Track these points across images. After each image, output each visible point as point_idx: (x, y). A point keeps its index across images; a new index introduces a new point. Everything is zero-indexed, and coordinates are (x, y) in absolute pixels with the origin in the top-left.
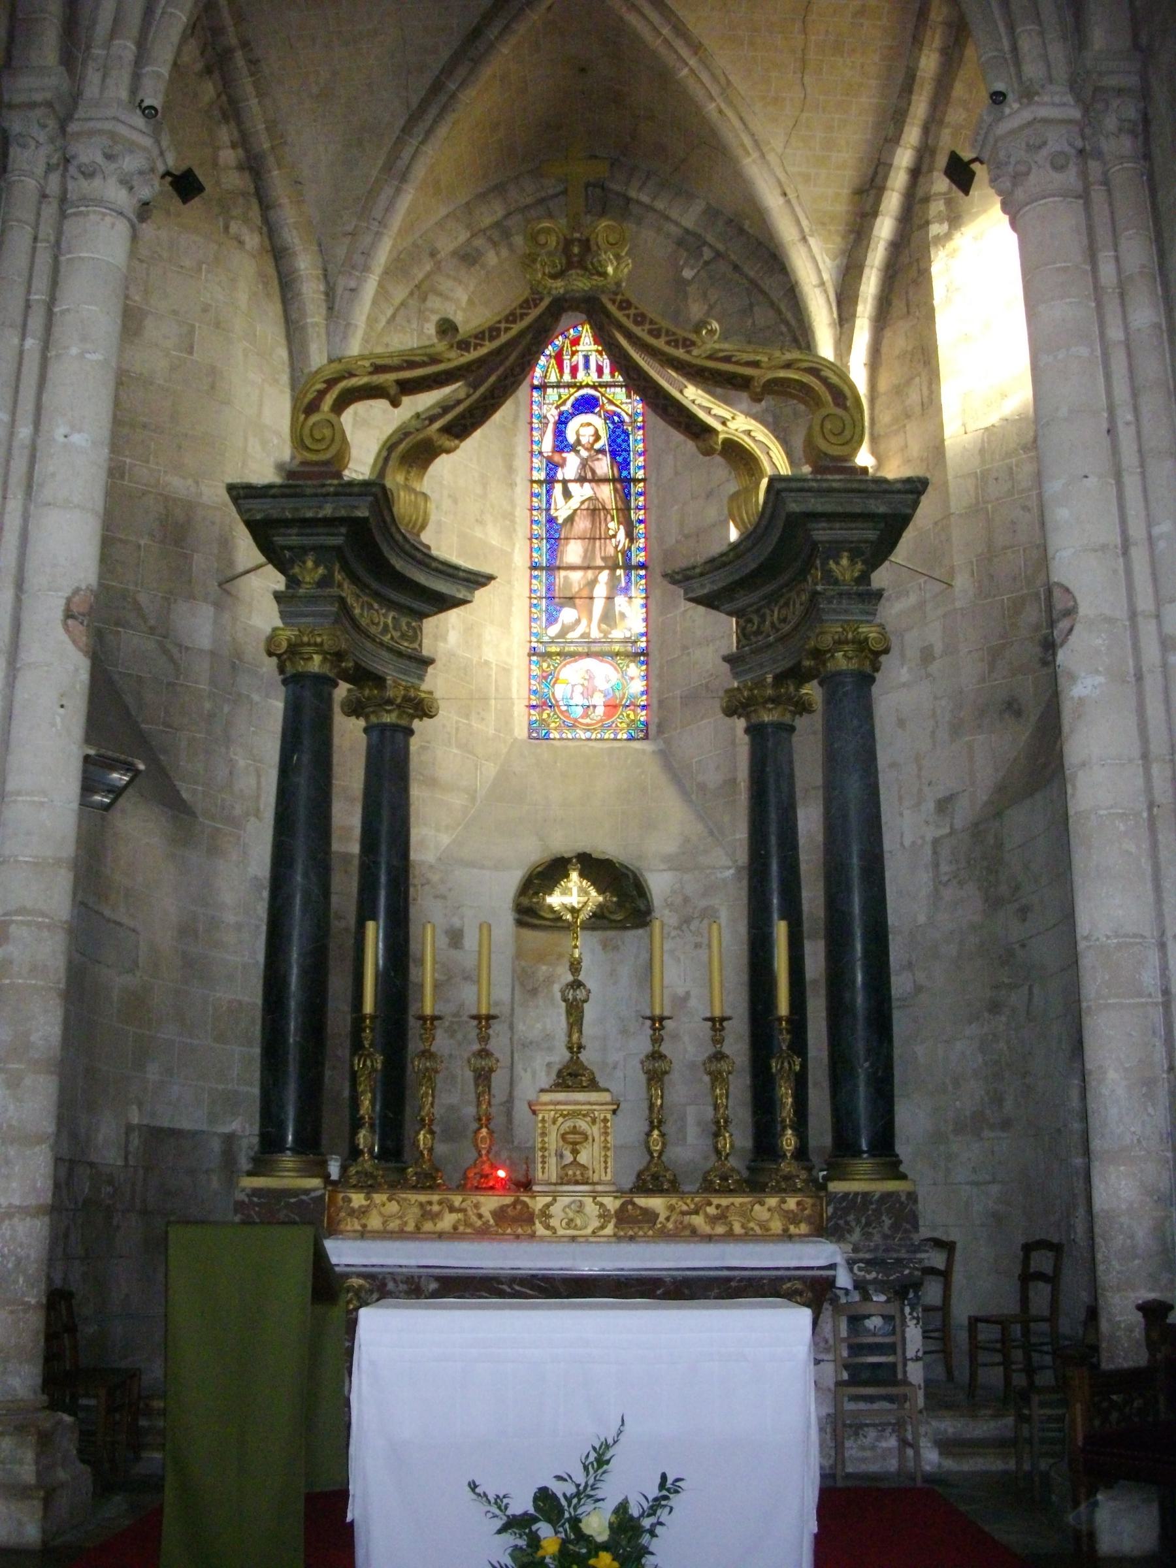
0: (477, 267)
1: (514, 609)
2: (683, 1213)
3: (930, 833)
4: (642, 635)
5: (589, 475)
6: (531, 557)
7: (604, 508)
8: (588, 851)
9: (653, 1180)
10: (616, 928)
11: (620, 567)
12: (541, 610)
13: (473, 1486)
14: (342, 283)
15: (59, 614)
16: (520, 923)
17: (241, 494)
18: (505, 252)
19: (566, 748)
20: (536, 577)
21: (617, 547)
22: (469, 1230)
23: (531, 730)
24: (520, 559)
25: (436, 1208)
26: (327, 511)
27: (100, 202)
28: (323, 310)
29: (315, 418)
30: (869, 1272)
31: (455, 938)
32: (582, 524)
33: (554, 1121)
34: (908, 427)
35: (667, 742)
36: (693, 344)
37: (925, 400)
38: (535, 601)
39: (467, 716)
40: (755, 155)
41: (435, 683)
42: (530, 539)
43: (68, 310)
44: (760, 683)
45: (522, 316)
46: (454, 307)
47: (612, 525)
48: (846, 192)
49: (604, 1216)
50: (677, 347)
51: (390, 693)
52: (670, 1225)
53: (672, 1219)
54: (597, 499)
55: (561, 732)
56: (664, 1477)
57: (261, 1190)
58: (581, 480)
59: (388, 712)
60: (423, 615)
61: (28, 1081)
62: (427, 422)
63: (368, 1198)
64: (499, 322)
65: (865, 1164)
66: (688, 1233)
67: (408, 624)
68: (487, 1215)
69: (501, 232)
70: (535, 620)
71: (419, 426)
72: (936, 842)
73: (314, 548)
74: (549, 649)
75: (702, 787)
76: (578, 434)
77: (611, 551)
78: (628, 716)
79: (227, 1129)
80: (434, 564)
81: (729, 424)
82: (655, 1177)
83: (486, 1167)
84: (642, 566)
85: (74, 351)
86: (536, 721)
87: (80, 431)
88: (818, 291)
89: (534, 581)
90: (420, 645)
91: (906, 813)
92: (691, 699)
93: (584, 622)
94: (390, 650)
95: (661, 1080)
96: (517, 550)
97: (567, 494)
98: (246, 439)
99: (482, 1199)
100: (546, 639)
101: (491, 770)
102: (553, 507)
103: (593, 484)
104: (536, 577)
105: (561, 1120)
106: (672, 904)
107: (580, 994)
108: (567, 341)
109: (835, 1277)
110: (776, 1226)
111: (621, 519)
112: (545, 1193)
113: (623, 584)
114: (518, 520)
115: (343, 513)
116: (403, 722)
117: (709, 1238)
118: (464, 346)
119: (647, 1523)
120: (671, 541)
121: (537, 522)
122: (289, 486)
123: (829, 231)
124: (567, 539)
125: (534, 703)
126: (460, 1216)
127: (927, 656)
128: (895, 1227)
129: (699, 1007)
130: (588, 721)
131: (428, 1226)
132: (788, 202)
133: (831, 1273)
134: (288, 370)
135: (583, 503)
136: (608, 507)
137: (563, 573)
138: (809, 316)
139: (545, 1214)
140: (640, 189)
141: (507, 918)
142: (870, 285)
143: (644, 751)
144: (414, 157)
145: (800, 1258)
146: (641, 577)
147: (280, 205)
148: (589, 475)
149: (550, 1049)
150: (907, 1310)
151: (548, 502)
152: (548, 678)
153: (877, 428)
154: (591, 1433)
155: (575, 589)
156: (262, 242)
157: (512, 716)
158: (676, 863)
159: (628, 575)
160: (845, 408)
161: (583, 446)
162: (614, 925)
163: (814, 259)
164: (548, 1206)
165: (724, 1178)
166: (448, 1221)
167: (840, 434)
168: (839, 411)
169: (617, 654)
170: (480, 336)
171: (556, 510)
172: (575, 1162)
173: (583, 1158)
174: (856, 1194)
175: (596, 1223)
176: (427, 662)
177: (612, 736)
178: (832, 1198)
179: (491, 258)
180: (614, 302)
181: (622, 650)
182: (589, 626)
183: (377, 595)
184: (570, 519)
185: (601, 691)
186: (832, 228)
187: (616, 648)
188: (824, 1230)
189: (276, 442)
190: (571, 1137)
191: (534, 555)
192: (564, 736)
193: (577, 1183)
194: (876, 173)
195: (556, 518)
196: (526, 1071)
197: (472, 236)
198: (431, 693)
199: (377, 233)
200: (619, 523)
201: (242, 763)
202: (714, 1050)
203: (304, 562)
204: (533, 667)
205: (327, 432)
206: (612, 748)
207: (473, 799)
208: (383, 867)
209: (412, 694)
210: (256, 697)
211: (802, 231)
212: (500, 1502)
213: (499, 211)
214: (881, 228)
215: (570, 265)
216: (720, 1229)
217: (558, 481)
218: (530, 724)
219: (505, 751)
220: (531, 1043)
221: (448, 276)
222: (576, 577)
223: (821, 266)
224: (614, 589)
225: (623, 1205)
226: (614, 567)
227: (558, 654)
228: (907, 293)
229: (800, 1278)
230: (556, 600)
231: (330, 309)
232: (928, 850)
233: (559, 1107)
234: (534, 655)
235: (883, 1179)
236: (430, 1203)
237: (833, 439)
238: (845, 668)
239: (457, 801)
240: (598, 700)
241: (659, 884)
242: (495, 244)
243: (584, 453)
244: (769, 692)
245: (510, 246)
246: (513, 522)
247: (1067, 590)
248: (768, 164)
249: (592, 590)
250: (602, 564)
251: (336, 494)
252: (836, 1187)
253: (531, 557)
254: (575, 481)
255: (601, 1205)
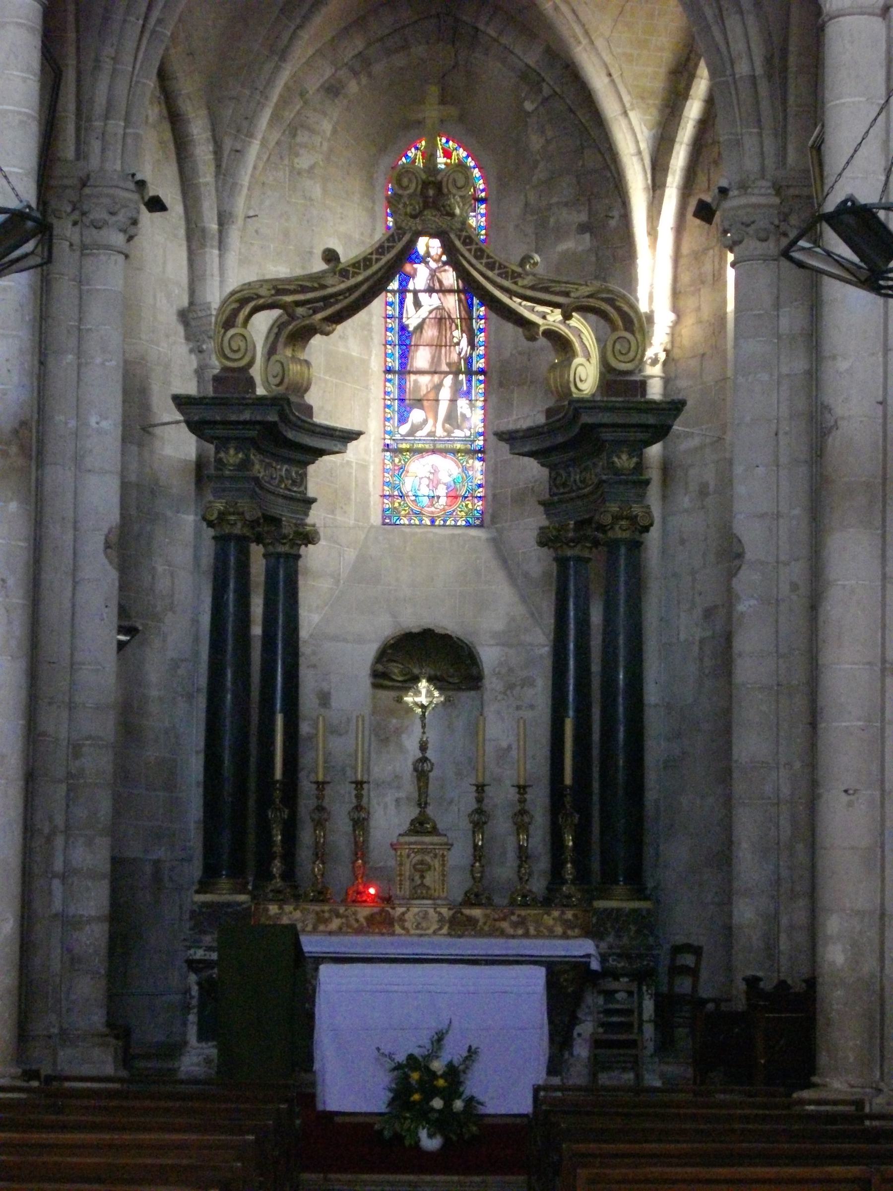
0: (341, 97)
1: (371, 411)
2: (495, 920)
3: (698, 634)
4: (481, 434)
5: (437, 286)
6: (386, 361)
7: (450, 317)
8: (431, 627)
9: (473, 899)
10: (454, 690)
11: (462, 373)
12: (394, 411)
13: (378, 1049)
14: (228, 144)
15: (101, 546)
16: (375, 686)
17: (181, 402)
18: (364, 80)
19: (415, 534)
20: (389, 381)
21: (460, 354)
22: (349, 930)
23: (384, 517)
24: (376, 365)
25: (327, 915)
26: (246, 416)
27: (108, 247)
28: (212, 169)
29: (232, 332)
30: (619, 963)
31: (324, 699)
32: (430, 332)
33: (408, 856)
34: (702, 291)
35: (500, 531)
36: (519, 275)
37: (716, 273)
38: (389, 403)
39: (333, 512)
40: (585, 42)
41: (316, 516)
42: (385, 345)
43: (90, 329)
44: (563, 527)
45: (390, 249)
46: (320, 140)
47: (457, 333)
48: (663, 71)
49: (441, 920)
50: (506, 278)
51: (285, 531)
52: (486, 928)
53: (488, 924)
54: (443, 308)
55: (410, 519)
56: (470, 1047)
57: (207, 903)
58: (430, 290)
59: (284, 544)
60: (306, 464)
61: (97, 840)
62: (311, 311)
63: (281, 908)
64: (371, 254)
65: (620, 889)
66: (498, 933)
67: (297, 473)
68: (362, 920)
69: (362, 64)
70: (388, 420)
71: (305, 314)
72: (702, 641)
73: (237, 439)
74: (400, 446)
75: (526, 575)
76: (428, 247)
77: (454, 357)
78: (467, 506)
79: (155, 857)
80: (318, 430)
81: (548, 317)
82: (477, 895)
83: (361, 887)
84: (481, 372)
85: (98, 360)
86: (389, 509)
87: (106, 418)
88: (635, 159)
89: (388, 384)
90: (306, 488)
91: (682, 614)
92: (519, 499)
93: (431, 422)
94: (285, 497)
95: (482, 828)
96: (373, 357)
97: (417, 304)
98: (155, 297)
99: (359, 909)
100: (398, 437)
101: (351, 555)
102: (404, 315)
103: (441, 295)
104: (389, 381)
105: (413, 855)
106: (499, 673)
107: (426, 767)
108: (419, 153)
109: (590, 962)
110: (559, 930)
111: (464, 328)
112: (400, 905)
113: (465, 388)
114: (374, 329)
115: (259, 418)
116: (293, 551)
117: (513, 937)
118: (344, 274)
119: (462, 1067)
120: (507, 354)
121: (391, 330)
122: (216, 398)
123: (648, 104)
124: (417, 345)
125: (387, 493)
126: (344, 920)
127: (703, 492)
128: (638, 932)
129: (510, 776)
130: (433, 509)
131: (322, 927)
132: (613, 81)
133: (588, 960)
134: (183, 223)
135: (431, 312)
136: (453, 316)
137: (413, 377)
138: (626, 184)
139: (402, 919)
140: (487, 24)
141: (365, 680)
142: (679, 158)
143: (479, 539)
144: (291, 39)
145: (567, 950)
146: (481, 382)
147: (176, 78)
148: (437, 286)
149: (399, 788)
150: (645, 988)
151: (401, 313)
152: (401, 470)
153: (679, 285)
154: (433, 1024)
155: (423, 391)
156: (160, 111)
157: (368, 506)
158: (506, 640)
159: (469, 381)
160: (633, 332)
161: (432, 258)
162: (451, 686)
163: (632, 129)
164: (403, 914)
165: (524, 896)
166: (335, 924)
167: (625, 354)
168: (627, 335)
169: (459, 451)
170: (356, 265)
171: (408, 318)
172: (422, 885)
173: (428, 881)
174: (612, 909)
175: (435, 926)
176: (311, 501)
177: (453, 523)
178: (596, 911)
179: (353, 87)
180: (459, 238)
181: (463, 447)
182: (435, 425)
183: (273, 455)
184: (420, 327)
185: (445, 484)
186: (651, 102)
187: (458, 446)
188: (588, 933)
189: (177, 291)
190: (419, 867)
191: (388, 360)
192: (412, 522)
193: (423, 898)
194: (688, 59)
195: (408, 326)
196: (379, 804)
197: (336, 71)
198: (314, 526)
199: (259, 103)
200: (462, 332)
201: (160, 569)
202: (519, 808)
203: (228, 449)
204: (386, 462)
205: (242, 344)
206: (453, 535)
207: (337, 582)
208: (280, 662)
209: (301, 530)
210: (169, 513)
211: (624, 106)
212: (390, 1056)
213: (359, 44)
214: (690, 110)
215: (426, 206)
216: (520, 932)
217: (409, 291)
218: (384, 511)
219: (363, 536)
220: (383, 782)
221: (315, 110)
222: (425, 381)
223: (639, 137)
224: (457, 392)
225: (454, 914)
226: (457, 373)
227: (408, 450)
228: (709, 170)
229: (567, 963)
230: (405, 403)
231: (218, 166)
232: (696, 648)
233: (412, 846)
234: (387, 451)
235: (633, 900)
236: (323, 912)
237: (621, 358)
238: (620, 536)
239: (325, 585)
240: (442, 491)
241: (489, 656)
242: (356, 74)
243: (433, 265)
244: (571, 534)
245: (370, 75)
246: (370, 331)
247: (740, 541)
248: (596, 49)
249: (437, 394)
250: (447, 369)
251: (253, 404)
252: (600, 904)
253: (386, 361)
254: (425, 291)
255: (440, 913)
